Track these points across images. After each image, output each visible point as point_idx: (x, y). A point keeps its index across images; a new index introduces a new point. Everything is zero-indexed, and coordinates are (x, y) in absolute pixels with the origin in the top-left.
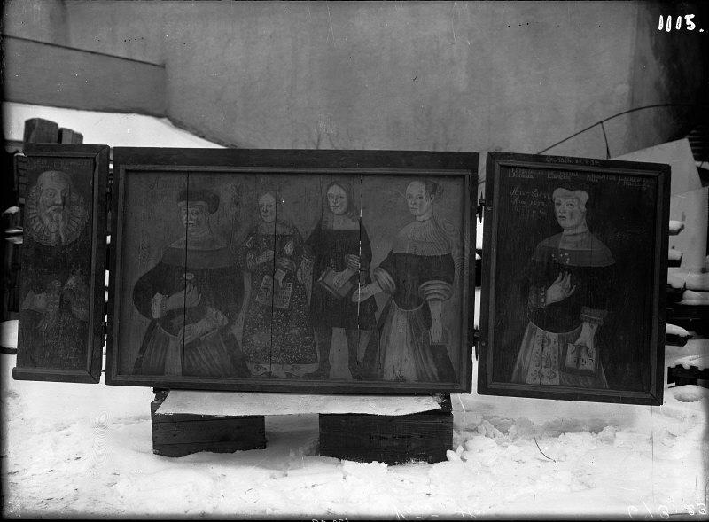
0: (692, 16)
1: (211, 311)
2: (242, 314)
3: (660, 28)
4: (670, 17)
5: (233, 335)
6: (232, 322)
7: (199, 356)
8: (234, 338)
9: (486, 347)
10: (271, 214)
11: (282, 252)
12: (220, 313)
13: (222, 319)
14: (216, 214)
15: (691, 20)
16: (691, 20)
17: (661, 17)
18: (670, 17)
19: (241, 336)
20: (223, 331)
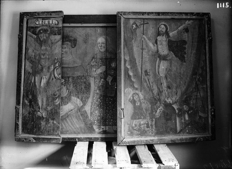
0: (228, 3)
1: (74, 98)
2: (90, 100)
3: (218, 7)
4: (224, 4)
5: (85, 111)
6: (84, 104)
7: (67, 123)
8: (86, 113)
9: (78, 138)
10: (104, 47)
11: (110, 66)
12: (78, 100)
13: (79, 102)
14: (75, 48)
15: (227, 4)
16: (227, 4)
17: (218, 4)
18: (224, 4)
19: (89, 111)
20: (80, 109)
